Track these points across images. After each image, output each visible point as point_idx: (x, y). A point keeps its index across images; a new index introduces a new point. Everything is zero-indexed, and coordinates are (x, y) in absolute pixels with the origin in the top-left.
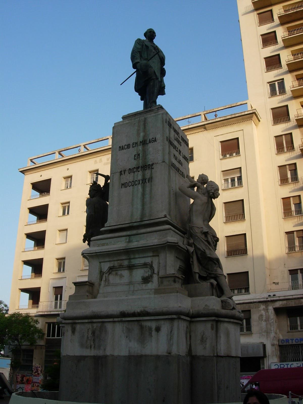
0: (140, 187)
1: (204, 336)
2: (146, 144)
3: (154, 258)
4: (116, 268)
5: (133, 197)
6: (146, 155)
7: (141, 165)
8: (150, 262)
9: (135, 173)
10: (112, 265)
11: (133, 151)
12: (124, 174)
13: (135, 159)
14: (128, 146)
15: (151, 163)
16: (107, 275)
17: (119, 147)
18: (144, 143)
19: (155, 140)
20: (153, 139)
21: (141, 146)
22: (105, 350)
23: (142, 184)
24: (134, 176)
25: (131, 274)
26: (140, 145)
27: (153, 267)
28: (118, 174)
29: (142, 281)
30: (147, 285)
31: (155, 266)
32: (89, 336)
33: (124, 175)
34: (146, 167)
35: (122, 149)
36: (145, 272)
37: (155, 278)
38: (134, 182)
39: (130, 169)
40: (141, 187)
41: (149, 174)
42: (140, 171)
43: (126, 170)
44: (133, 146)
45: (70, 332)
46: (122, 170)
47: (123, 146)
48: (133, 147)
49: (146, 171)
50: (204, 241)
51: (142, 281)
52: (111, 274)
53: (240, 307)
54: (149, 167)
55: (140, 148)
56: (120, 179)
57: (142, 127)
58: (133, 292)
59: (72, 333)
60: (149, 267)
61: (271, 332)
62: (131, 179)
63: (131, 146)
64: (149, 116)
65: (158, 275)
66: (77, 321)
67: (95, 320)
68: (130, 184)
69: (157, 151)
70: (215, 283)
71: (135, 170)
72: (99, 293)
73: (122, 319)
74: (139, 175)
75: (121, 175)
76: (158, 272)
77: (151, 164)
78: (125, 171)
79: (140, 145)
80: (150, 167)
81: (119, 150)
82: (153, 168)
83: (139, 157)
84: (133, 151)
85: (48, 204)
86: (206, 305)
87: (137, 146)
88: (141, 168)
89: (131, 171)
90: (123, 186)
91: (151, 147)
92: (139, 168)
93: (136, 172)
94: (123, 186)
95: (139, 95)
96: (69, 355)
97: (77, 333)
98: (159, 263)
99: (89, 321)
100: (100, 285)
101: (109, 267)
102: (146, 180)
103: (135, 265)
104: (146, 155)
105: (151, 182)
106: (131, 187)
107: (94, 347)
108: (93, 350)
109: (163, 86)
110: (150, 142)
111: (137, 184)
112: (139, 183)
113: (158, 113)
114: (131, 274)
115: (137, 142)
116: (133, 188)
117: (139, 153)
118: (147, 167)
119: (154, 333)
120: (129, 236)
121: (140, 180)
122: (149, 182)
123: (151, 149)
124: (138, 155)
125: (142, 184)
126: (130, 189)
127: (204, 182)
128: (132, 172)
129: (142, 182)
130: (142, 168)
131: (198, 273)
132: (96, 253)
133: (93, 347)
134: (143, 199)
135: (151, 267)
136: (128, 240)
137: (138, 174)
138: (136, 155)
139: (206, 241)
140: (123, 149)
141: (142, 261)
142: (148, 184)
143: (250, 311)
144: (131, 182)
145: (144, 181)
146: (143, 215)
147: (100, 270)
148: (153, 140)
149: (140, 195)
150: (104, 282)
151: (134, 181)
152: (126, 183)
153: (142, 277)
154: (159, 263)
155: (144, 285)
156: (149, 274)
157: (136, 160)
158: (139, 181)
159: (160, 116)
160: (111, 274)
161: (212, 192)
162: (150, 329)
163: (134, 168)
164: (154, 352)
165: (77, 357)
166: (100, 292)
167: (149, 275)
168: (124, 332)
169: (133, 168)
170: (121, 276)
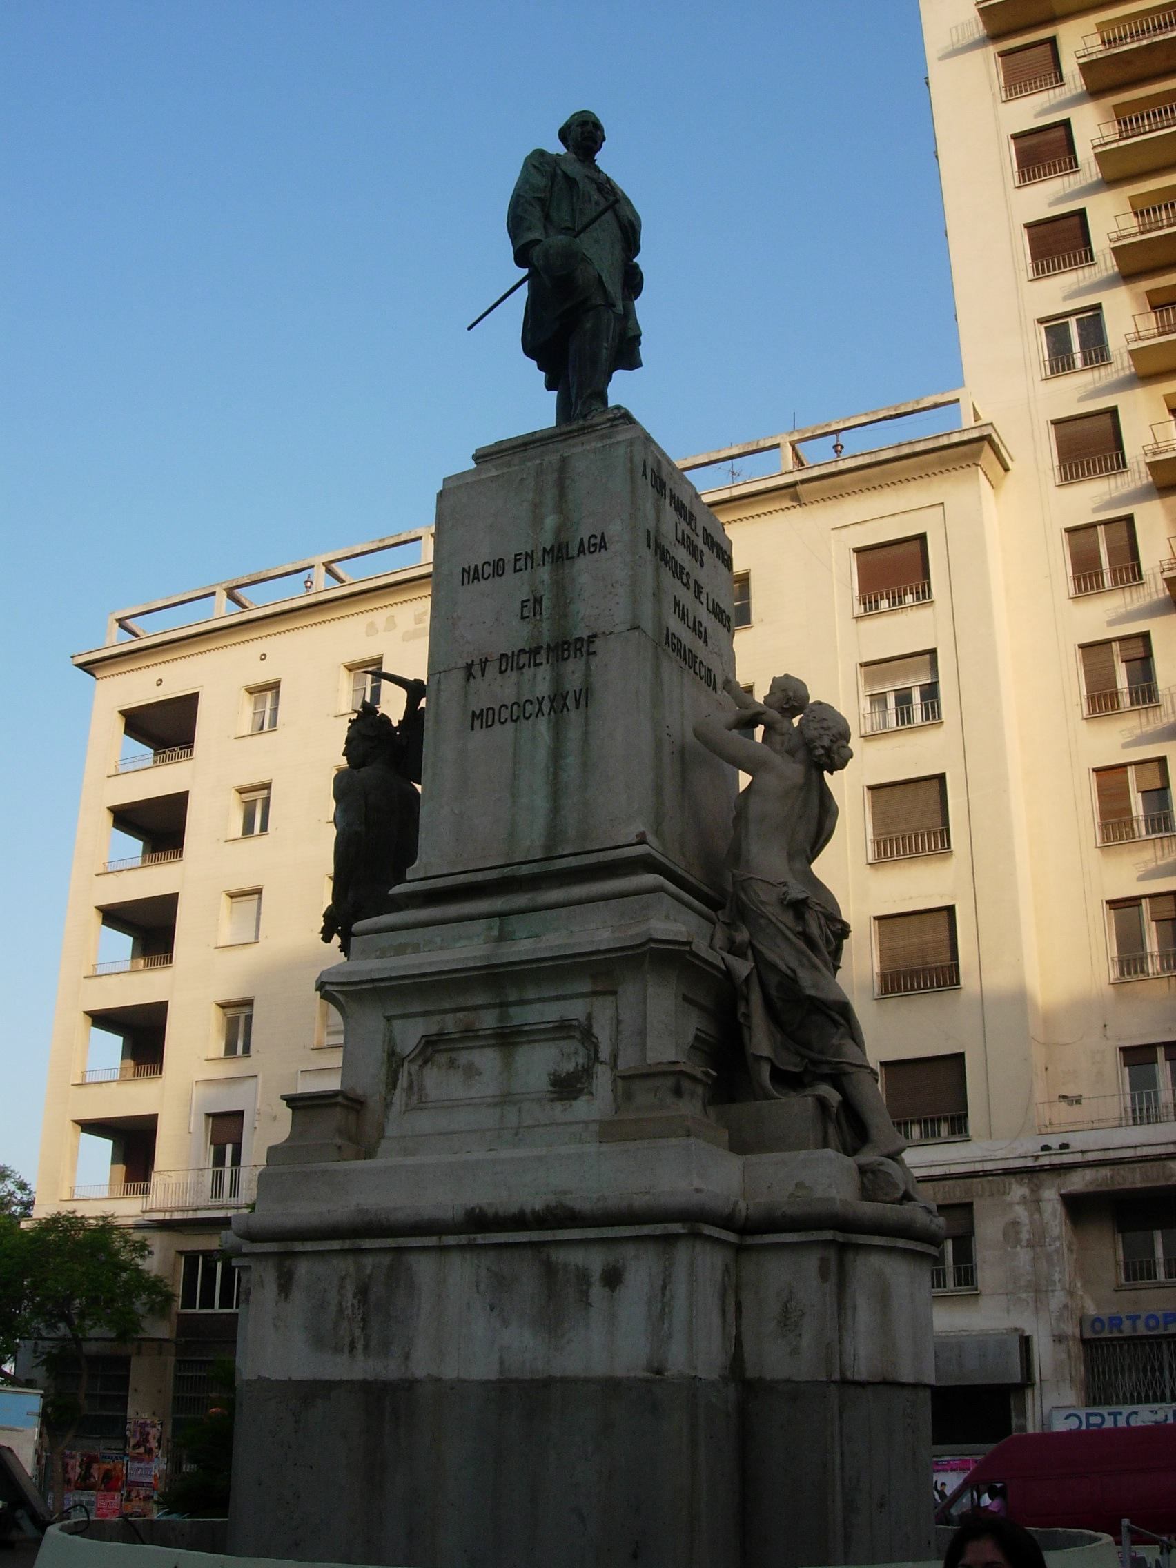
0: (543, 726)
2: (568, 559)
3: (598, 1001)
6: (568, 601)
7: (546, 639)
8: (583, 1019)
9: (522, 673)
10: (434, 1029)
11: (515, 587)
13: (523, 618)
14: (498, 568)
15: (585, 634)
16: (415, 1068)
17: (464, 569)
18: (559, 554)
19: (603, 545)
20: (593, 541)
21: (548, 567)
22: (407, 1357)
23: (552, 713)
24: (519, 684)
25: (508, 1063)
29: (552, 1092)
31: (603, 1033)
34: (566, 647)
37: (603, 1079)
38: (519, 706)
39: (503, 655)
42: (544, 661)
46: (473, 661)
47: (476, 566)
53: (931, 1192)
54: (580, 650)
55: (545, 573)
57: (550, 495)
60: (577, 1034)
61: (1050, 1288)
63: (509, 568)
64: (579, 449)
65: (614, 1066)
66: (299, 1247)
67: (367, 1244)
69: (610, 586)
70: (834, 1097)
72: (383, 1137)
74: (539, 678)
75: (471, 679)
76: (615, 1057)
77: (586, 638)
78: (484, 663)
79: (544, 564)
80: (584, 650)
81: (463, 584)
83: (538, 608)
84: (515, 587)
87: (532, 568)
89: (508, 662)
90: (477, 723)
91: (584, 570)
92: (539, 653)
93: (529, 667)
94: (477, 723)
95: (540, 368)
98: (618, 1020)
99: (347, 1244)
100: (388, 1105)
101: (423, 1036)
103: (526, 1028)
104: (568, 601)
106: (510, 726)
110: (581, 551)
112: (540, 709)
113: (613, 440)
114: (508, 1063)
117: (538, 595)
119: (597, 1292)
121: (544, 697)
122: (577, 707)
123: (584, 579)
124: (535, 600)
125: (549, 714)
126: (503, 733)
127: (793, 705)
128: (512, 670)
129: (552, 707)
130: (551, 654)
131: (768, 1059)
135: (587, 1035)
136: (495, 933)
138: (528, 600)
139: (798, 934)
140: (476, 578)
141: (552, 1012)
142: (574, 716)
143: (969, 1206)
145: (558, 701)
146: (554, 834)
148: (595, 545)
149: (542, 756)
152: (490, 712)
153: (549, 1075)
154: (618, 1022)
155: (559, 1106)
157: (527, 620)
158: (540, 703)
159: (621, 450)
160: (429, 1065)
161: (823, 747)
163: (522, 651)
164: (599, 1367)
166: (387, 1134)
168: (482, 1287)
169: (516, 653)
170: (471, 1072)
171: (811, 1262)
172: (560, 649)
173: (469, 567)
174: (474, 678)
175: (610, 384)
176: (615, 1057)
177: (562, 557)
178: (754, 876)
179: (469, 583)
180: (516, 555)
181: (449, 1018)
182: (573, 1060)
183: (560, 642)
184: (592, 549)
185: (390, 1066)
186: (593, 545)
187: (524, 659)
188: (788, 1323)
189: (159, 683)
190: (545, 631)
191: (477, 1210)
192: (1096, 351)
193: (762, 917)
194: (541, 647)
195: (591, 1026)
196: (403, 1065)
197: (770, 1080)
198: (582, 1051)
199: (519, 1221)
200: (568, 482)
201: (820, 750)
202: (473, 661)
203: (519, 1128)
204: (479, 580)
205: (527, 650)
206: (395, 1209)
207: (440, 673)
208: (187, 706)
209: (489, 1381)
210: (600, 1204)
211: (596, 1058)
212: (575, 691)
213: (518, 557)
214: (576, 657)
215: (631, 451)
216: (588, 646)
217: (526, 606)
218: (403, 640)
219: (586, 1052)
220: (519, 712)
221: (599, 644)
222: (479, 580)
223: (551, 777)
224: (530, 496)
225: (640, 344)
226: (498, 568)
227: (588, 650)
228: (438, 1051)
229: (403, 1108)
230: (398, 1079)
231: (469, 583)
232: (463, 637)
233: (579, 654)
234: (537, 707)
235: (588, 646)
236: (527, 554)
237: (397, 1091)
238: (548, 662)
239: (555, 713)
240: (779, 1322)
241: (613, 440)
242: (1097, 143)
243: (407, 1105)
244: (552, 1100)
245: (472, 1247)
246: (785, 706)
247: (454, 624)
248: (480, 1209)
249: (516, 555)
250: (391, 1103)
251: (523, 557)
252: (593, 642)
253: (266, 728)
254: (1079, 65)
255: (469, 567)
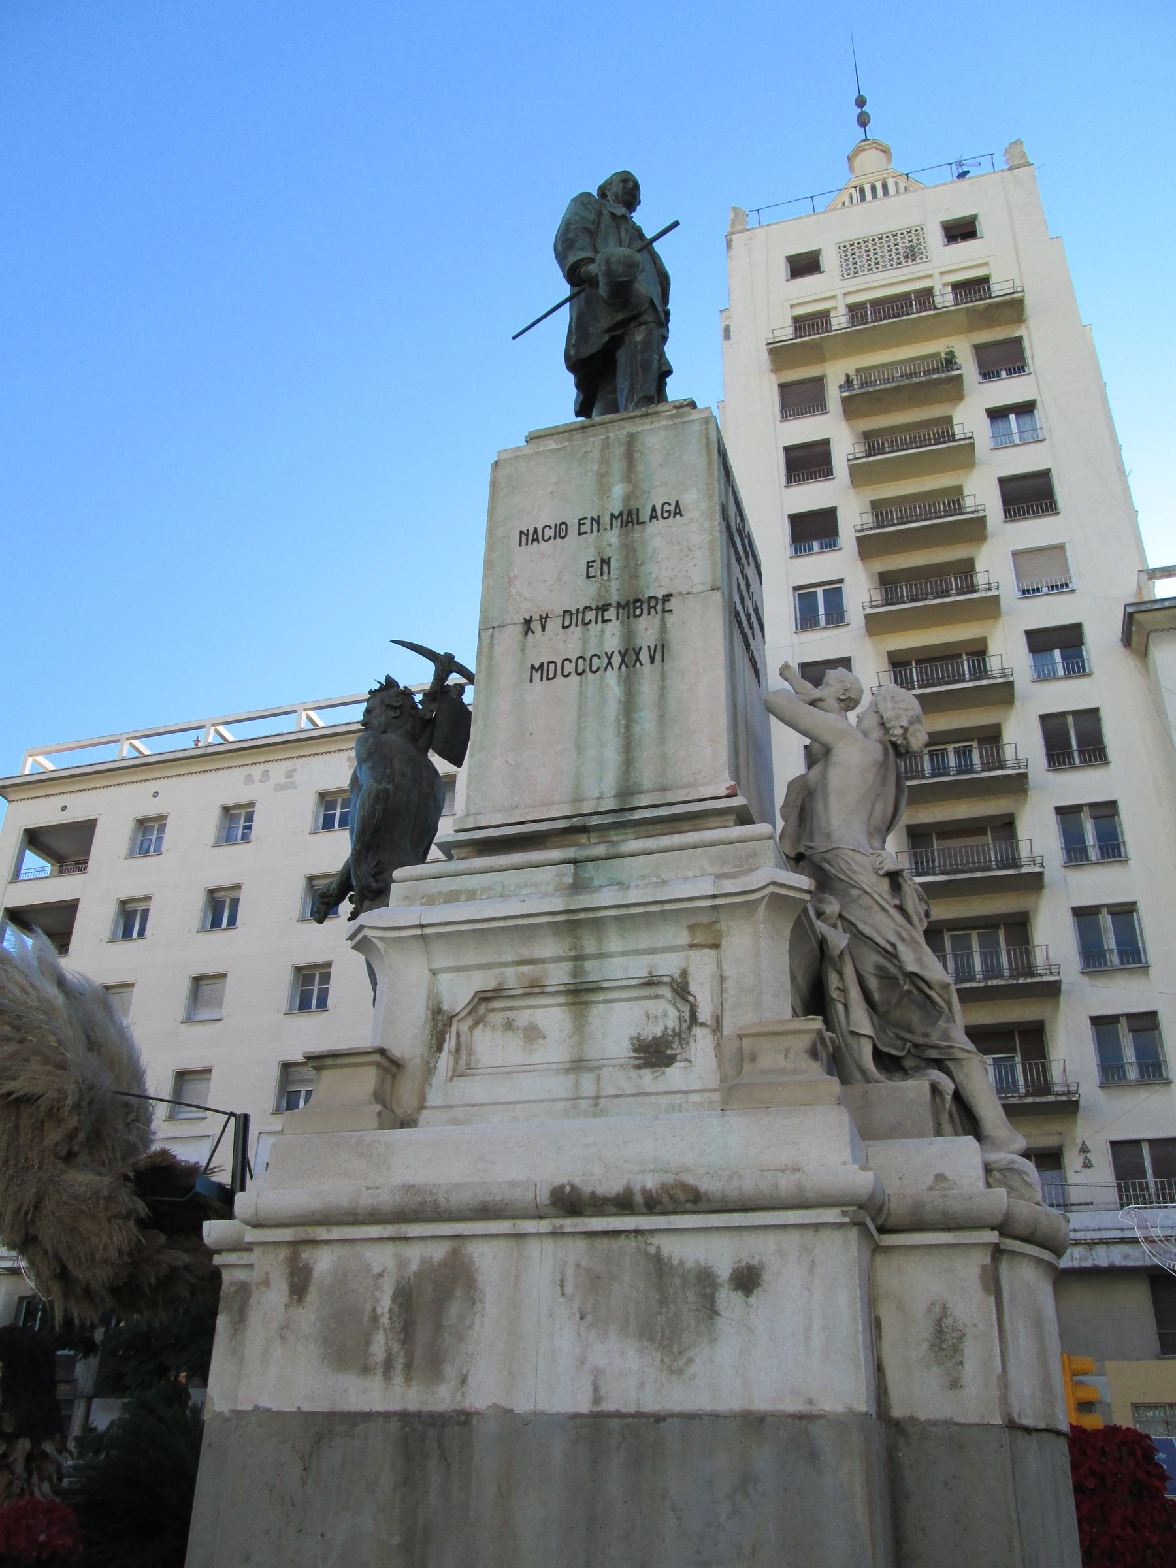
0: (612, 678)
1: (949, 1321)
2: (638, 523)
3: (695, 955)
4: (513, 997)
5: (580, 717)
6: (639, 563)
7: (614, 598)
8: (677, 974)
9: (588, 630)
10: (492, 984)
11: (580, 549)
12: (543, 630)
13: (588, 577)
14: (560, 531)
15: (659, 594)
16: (464, 1027)
17: (521, 532)
18: (629, 519)
19: (678, 511)
20: (666, 507)
21: (616, 531)
23: (623, 667)
24: (585, 641)
25: (580, 1026)
26: (611, 528)
27: (689, 994)
28: (520, 629)
29: (636, 1058)
30: (664, 1073)
32: (379, 1310)
33: (541, 633)
34: (638, 604)
35: (533, 540)
36: (648, 1017)
37: (702, 1044)
38: (585, 659)
39: (565, 612)
40: (619, 682)
41: (650, 631)
42: (614, 618)
43: (550, 615)
44: (582, 532)
45: (274, 1297)
46: (531, 617)
47: (535, 530)
48: (580, 534)
49: (641, 619)
50: (887, 907)
51: (636, 1055)
52: (484, 1025)
54: (654, 607)
55: (613, 537)
56: (523, 650)
57: (617, 467)
58: (596, 1105)
59: (291, 1296)
60: (667, 992)
62: (573, 651)
63: (573, 531)
64: (648, 427)
65: (717, 1027)
66: (322, 1233)
67: (415, 1230)
68: (569, 667)
69: (686, 550)
70: (948, 1086)
71: (590, 615)
72: (424, 1108)
73: (561, 1226)
74: (608, 634)
75: (530, 633)
76: (718, 1020)
77: (660, 597)
78: (544, 620)
79: (611, 528)
80: (659, 608)
81: (520, 545)
82: (671, 610)
83: (605, 569)
84: (580, 549)
85: (96, 820)
86: (940, 1178)
87: (598, 531)
88: (618, 609)
90: (537, 675)
91: (656, 535)
92: (607, 610)
93: (596, 623)
95: (578, 386)
96: (269, 1410)
97: (312, 1296)
98: (721, 976)
99: (389, 1230)
100: (429, 1070)
101: (477, 992)
102: (638, 654)
103: (605, 985)
104: (639, 563)
105: (663, 661)
106: (574, 678)
107: (408, 1366)
108: (398, 1379)
109: (665, 369)
110: (653, 516)
111: (598, 669)
112: (609, 663)
113: (685, 419)
114: (580, 1026)
115: (599, 517)
116: (581, 682)
117: (605, 557)
118: (645, 607)
119: (728, 1299)
120: (574, 861)
121: (613, 652)
122: (652, 661)
123: (657, 542)
124: (603, 561)
125: (620, 668)
127: (849, 697)
128: (576, 625)
129: (623, 661)
130: (621, 611)
131: (870, 1037)
132: (422, 926)
133: (399, 1362)
134: (628, 728)
135: (681, 989)
136: (569, 880)
137: (603, 631)
138: (594, 561)
139: (896, 906)
140: (535, 539)
141: (638, 968)
142: (647, 670)
144: (571, 662)
145: (630, 656)
146: (626, 791)
147: (430, 1003)
148: (669, 511)
149: (613, 708)
150: (451, 1059)
151: (588, 657)
152: (552, 666)
153: (631, 1039)
155: (647, 1073)
156: (666, 1028)
157: (593, 579)
158: (609, 658)
159: (696, 427)
160: (481, 1026)
161: (902, 727)
162: (705, 1279)
164: (729, 1400)
165: (309, 1417)
166: (428, 1104)
167: (670, 1032)
168: (569, 1289)
169: (581, 610)
170: (533, 1034)
171: (970, 1268)
172: (632, 607)
173: (528, 530)
174: (533, 632)
175: (667, 389)
176: (718, 1020)
177: (632, 522)
178: (841, 846)
179: (527, 544)
180: (580, 520)
181: (510, 972)
182: (661, 1021)
183: (632, 601)
184: (666, 515)
185: (435, 1026)
186: (667, 511)
187: (590, 615)
188: (944, 1346)
189: (64, 808)
190: (614, 591)
191: (568, 1189)
192: (836, 616)
193: (855, 887)
194: (610, 605)
195: (687, 983)
196: (451, 1025)
197: (876, 1065)
198: (673, 1013)
199: (624, 1204)
200: (637, 455)
201: (899, 729)
202: (531, 617)
203: (598, 1097)
204: (538, 542)
205: (594, 606)
206: (457, 1186)
207: (494, 628)
208: (84, 831)
209: (577, 1416)
210: (735, 1183)
211: (694, 1019)
212: (649, 647)
213: (582, 522)
214: (649, 614)
215: (707, 429)
216: (664, 604)
217: (592, 566)
218: (275, 790)
219: (678, 1014)
220: (585, 665)
221: (672, 604)
222: (538, 542)
223: (622, 730)
224: (596, 467)
225: (666, 385)
226: (560, 531)
227: (663, 608)
228: (493, 1010)
229: (450, 1073)
230: (445, 1040)
231: (527, 544)
232: (519, 594)
233: (652, 611)
234: (606, 661)
235: (664, 604)
236: (592, 519)
237: (443, 1053)
238: (618, 619)
239: (627, 667)
240: (932, 1345)
241: (685, 419)
242: (851, 457)
243: (454, 1071)
244: (638, 1067)
245: (555, 1234)
246: (842, 697)
247: (510, 582)
248: (573, 1187)
249: (580, 520)
250: (435, 1067)
251: (588, 522)
252: (669, 600)
253: (151, 852)
254: (841, 397)
255: (528, 530)
